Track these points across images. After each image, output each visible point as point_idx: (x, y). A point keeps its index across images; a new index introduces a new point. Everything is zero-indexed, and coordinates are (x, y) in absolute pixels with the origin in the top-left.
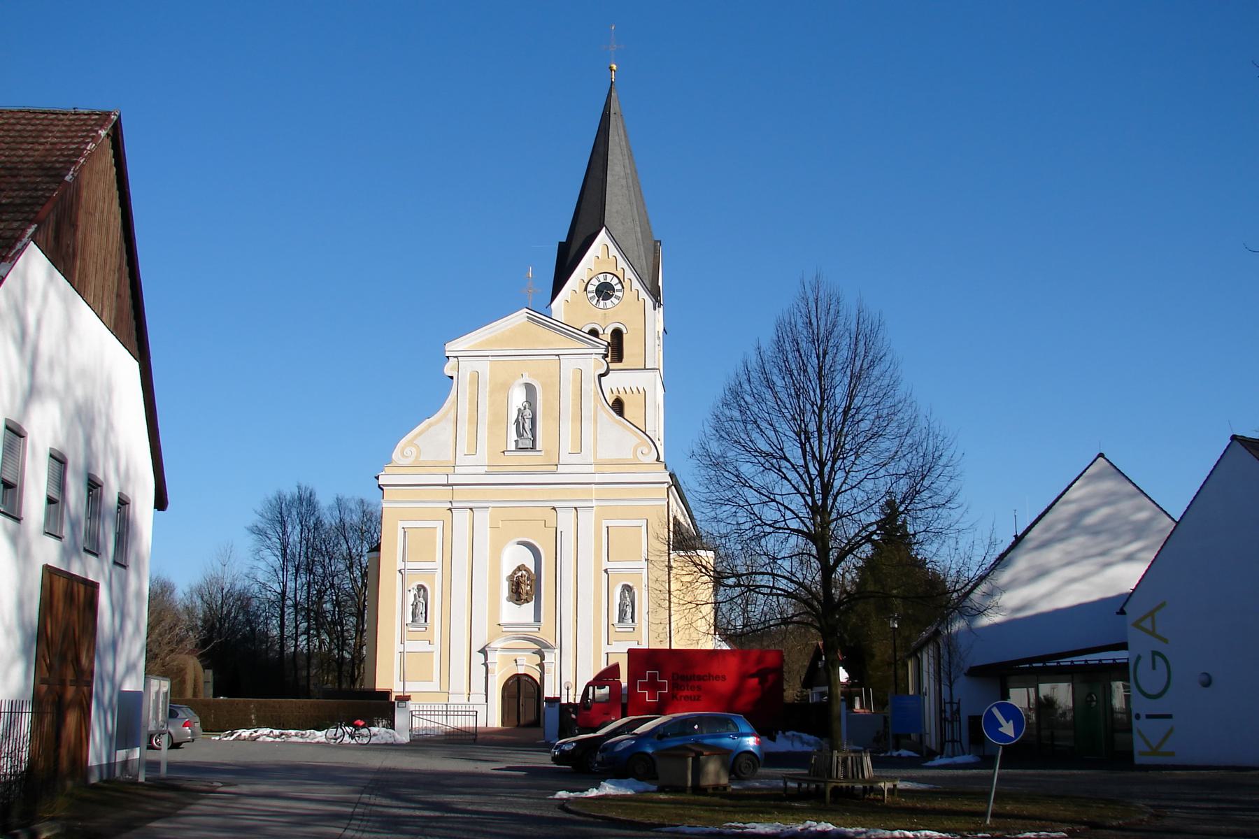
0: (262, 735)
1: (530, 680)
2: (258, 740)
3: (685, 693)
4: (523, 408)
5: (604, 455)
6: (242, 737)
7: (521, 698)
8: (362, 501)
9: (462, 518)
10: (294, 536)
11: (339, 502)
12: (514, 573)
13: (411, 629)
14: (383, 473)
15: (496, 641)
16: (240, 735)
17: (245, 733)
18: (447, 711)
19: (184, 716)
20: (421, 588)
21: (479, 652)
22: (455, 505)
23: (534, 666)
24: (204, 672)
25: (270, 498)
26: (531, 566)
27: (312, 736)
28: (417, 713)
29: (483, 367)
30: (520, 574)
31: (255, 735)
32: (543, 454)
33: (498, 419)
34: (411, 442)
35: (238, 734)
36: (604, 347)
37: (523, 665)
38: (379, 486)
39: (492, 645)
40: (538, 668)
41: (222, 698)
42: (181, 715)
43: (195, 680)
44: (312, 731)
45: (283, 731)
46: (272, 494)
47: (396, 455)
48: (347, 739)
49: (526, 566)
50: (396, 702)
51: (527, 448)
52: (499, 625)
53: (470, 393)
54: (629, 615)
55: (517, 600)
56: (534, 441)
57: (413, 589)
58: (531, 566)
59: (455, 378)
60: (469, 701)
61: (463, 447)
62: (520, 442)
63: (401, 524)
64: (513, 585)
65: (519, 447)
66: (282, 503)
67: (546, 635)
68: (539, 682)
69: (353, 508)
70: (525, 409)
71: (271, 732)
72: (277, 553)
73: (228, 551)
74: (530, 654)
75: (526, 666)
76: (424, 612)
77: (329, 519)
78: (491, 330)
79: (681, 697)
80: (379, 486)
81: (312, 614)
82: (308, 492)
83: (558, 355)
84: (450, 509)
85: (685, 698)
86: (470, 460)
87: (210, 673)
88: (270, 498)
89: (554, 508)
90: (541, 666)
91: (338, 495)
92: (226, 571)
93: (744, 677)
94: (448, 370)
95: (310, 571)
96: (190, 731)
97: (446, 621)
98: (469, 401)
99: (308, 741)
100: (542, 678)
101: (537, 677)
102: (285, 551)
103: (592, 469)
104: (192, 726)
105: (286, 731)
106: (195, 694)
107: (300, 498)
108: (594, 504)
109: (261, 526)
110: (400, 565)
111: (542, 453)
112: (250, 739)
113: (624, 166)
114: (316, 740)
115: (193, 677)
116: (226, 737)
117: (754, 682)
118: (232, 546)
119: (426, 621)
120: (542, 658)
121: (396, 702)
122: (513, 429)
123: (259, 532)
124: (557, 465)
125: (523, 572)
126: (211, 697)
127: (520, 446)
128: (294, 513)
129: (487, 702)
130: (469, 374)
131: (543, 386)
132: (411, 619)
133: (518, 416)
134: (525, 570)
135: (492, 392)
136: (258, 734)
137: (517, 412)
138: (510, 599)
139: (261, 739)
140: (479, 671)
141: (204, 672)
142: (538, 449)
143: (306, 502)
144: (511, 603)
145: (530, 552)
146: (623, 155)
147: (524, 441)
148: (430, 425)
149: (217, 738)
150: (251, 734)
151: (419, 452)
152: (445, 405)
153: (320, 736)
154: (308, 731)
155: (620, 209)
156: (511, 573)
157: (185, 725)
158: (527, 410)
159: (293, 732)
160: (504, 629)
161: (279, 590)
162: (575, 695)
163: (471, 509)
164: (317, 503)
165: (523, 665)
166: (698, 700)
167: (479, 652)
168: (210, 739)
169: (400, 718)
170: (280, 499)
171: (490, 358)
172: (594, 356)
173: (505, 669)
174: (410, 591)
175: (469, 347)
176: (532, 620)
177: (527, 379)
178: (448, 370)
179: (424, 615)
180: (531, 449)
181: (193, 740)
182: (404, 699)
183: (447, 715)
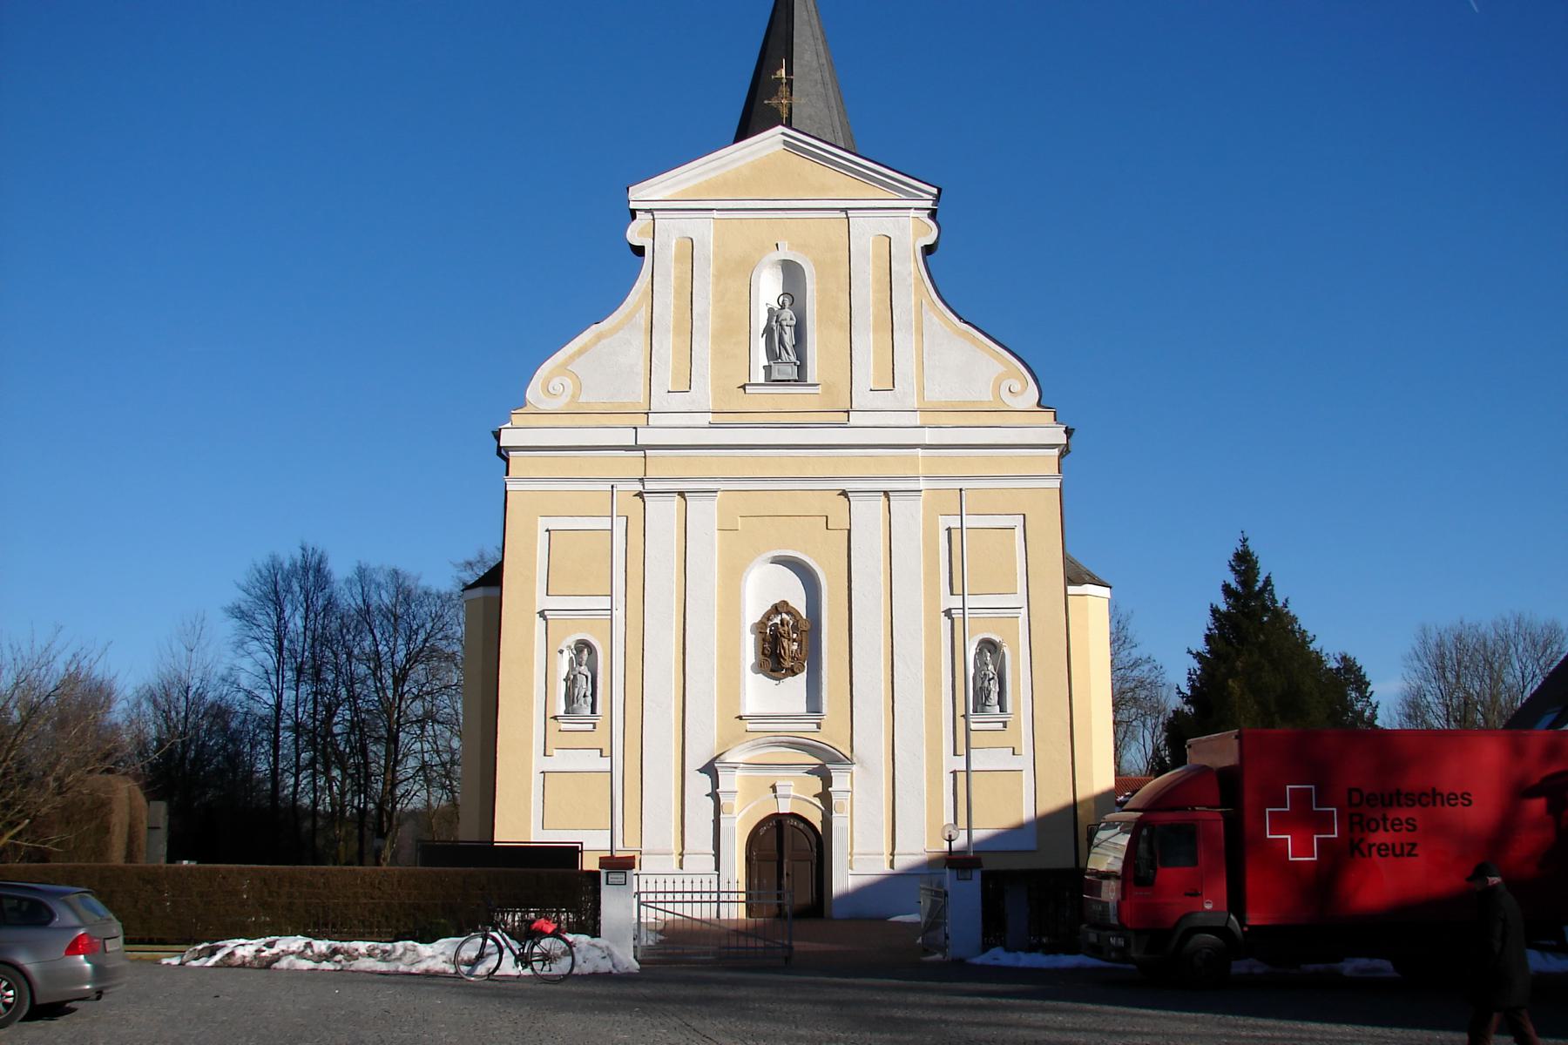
0: (286, 953)
1: (801, 826)
2: (276, 965)
3: (1381, 837)
4: (777, 307)
5: (937, 393)
6: (237, 959)
7: (785, 861)
8: (396, 573)
9: (663, 512)
10: (296, 623)
11: (362, 574)
12: (767, 617)
13: (563, 727)
14: (509, 425)
15: (737, 749)
16: (232, 954)
17: (245, 949)
18: (719, 892)
19: (74, 921)
20: (583, 646)
21: (701, 771)
22: (649, 486)
23: (810, 799)
24: (149, 805)
25: (260, 565)
26: (799, 603)
27: (409, 957)
28: (651, 897)
29: (703, 229)
30: (777, 620)
31: (267, 953)
32: (820, 391)
33: (731, 326)
34: (563, 368)
35: (226, 951)
36: (931, 197)
37: (787, 797)
38: (499, 448)
39: (728, 758)
40: (817, 802)
41: (185, 862)
42: (63, 916)
43: (131, 826)
44: (411, 942)
45: (338, 944)
46: (262, 559)
47: (533, 392)
48: (509, 967)
49: (790, 604)
50: (603, 872)
51: (789, 381)
52: (740, 718)
53: (676, 278)
54: (994, 697)
55: (772, 671)
56: (802, 368)
57: (569, 647)
58: (799, 603)
59: (648, 252)
60: (682, 868)
61: (664, 377)
62: (775, 368)
63: (543, 524)
64: (764, 640)
65: (773, 378)
66: (276, 576)
67: (831, 734)
68: (819, 827)
69: (383, 581)
70: (783, 307)
71: (309, 945)
72: (268, 646)
73: (198, 627)
74: (800, 774)
75: (795, 797)
76: (589, 693)
77: (348, 600)
78: (714, 164)
79: (1370, 846)
80: (499, 448)
81: (316, 737)
82: (317, 557)
83: (845, 210)
84: (640, 495)
85: (1379, 849)
86: (677, 402)
87: (161, 807)
88: (260, 565)
89: (844, 493)
90: (825, 797)
91: (359, 562)
92: (194, 660)
93: (1521, 791)
94: (635, 233)
95: (317, 677)
96: (88, 965)
97: (634, 710)
98: (676, 291)
99: (402, 968)
100: (827, 821)
101: (816, 818)
102: (281, 644)
103: (916, 419)
104: (95, 951)
105: (345, 944)
106: (130, 856)
107: (306, 570)
108: (922, 485)
109: (244, 607)
110: (543, 602)
111: (819, 390)
112: (256, 963)
113: (817, 53)
114: (422, 967)
115: (127, 820)
116: (196, 959)
117: (1537, 805)
118: (204, 620)
119: (593, 711)
120: (827, 781)
121: (603, 872)
122: (760, 344)
123: (240, 614)
124: (848, 412)
125: (784, 616)
126: (163, 860)
127: (775, 376)
128: (296, 588)
129: (717, 868)
130: (674, 241)
131: (816, 263)
132: (565, 708)
133: (769, 320)
134: (787, 613)
135: (719, 276)
136: (275, 950)
137: (767, 315)
138: (760, 668)
139: (284, 964)
140: (701, 810)
141: (149, 805)
142: (809, 382)
143: (313, 573)
144: (761, 675)
145: (797, 578)
146: (815, 39)
147: (782, 367)
148: (599, 337)
149: (175, 961)
150: (259, 951)
151: (579, 387)
152: (629, 299)
153: (435, 955)
154: (400, 945)
155: (813, 113)
156: (759, 619)
157: (73, 949)
158: (787, 310)
159: (362, 946)
160: (749, 727)
161: (271, 702)
162: (892, 854)
163: (681, 494)
164: (329, 572)
165: (787, 797)
166: (1409, 855)
167: (701, 771)
168: (157, 962)
169: (615, 906)
170: (274, 567)
171: (715, 214)
172: (912, 213)
173: (755, 803)
174: (561, 652)
175: (671, 196)
176: (801, 708)
177: (786, 253)
178: (635, 233)
179: (589, 699)
180: (796, 381)
181: (99, 994)
182: (620, 865)
183: (718, 902)
